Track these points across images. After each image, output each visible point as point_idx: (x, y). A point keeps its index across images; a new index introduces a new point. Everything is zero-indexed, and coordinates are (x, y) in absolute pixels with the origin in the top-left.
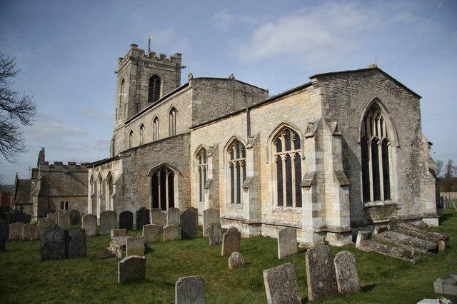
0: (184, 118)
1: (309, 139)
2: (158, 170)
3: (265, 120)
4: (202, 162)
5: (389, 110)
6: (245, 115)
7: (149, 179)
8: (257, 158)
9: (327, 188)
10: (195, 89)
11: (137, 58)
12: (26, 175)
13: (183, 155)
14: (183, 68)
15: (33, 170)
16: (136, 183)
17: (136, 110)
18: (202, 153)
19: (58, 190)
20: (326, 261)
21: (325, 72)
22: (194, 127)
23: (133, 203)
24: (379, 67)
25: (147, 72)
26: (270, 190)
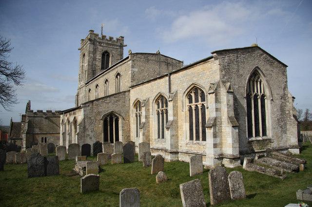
0: (126, 80)
1: (211, 95)
2: (108, 116)
3: (181, 82)
4: (138, 111)
5: (265, 75)
6: (167, 78)
7: (102, 122)
8: (175, 107)
9: (223, 128)
10: (133, 61)
11: (94, 40)
12: (18, 119)
13: (125, 105)
14: (125, 46)
15: (23, 116)
16: (93, 125)
17: (93, 75)
18: (138, 104)
19: (40, 130)
20: (223, 178)
21: (222, 49)
22: (133, 87)
23: (91, 138)
24: (259, 46)
25: (100, 49)
26: (184, 129)
